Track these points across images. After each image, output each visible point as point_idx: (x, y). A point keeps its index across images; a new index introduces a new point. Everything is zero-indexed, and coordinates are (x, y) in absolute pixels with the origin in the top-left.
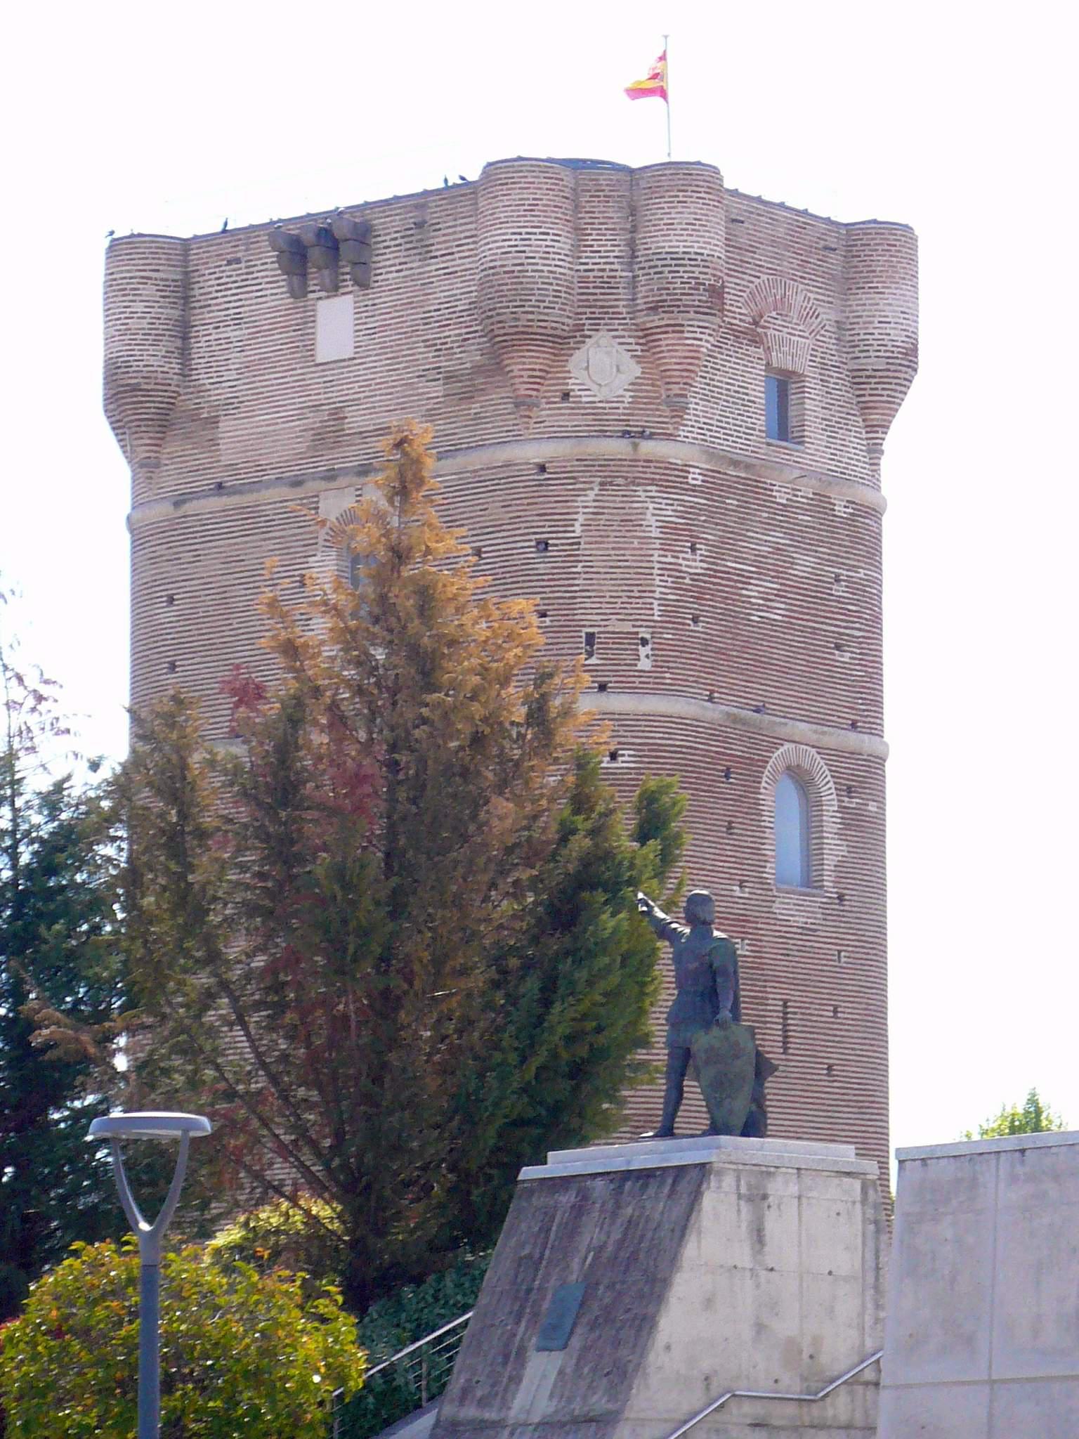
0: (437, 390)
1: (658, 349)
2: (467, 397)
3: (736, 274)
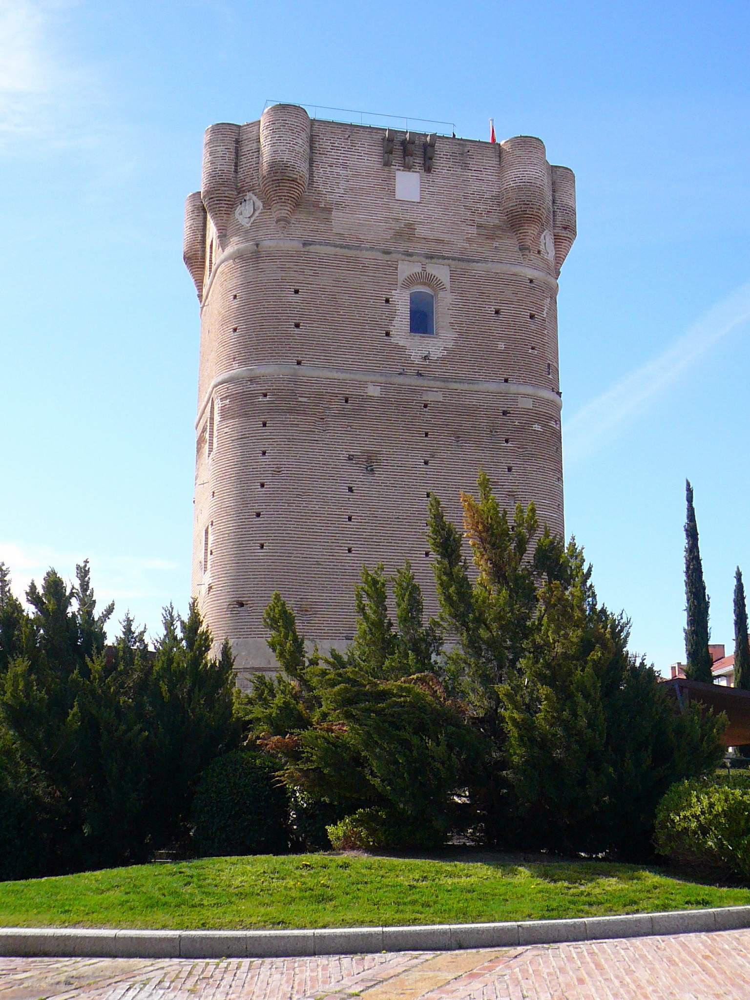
0: (474, 230)
1: (560, 246)
2: (491, 237)
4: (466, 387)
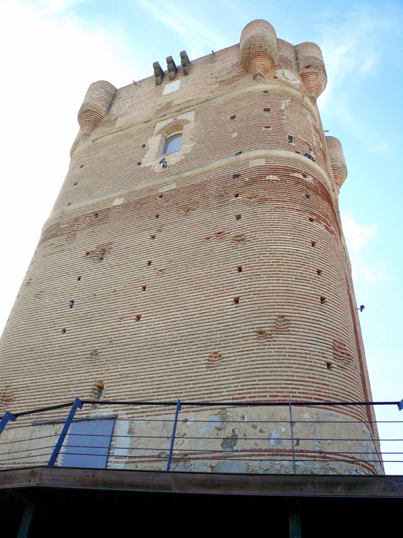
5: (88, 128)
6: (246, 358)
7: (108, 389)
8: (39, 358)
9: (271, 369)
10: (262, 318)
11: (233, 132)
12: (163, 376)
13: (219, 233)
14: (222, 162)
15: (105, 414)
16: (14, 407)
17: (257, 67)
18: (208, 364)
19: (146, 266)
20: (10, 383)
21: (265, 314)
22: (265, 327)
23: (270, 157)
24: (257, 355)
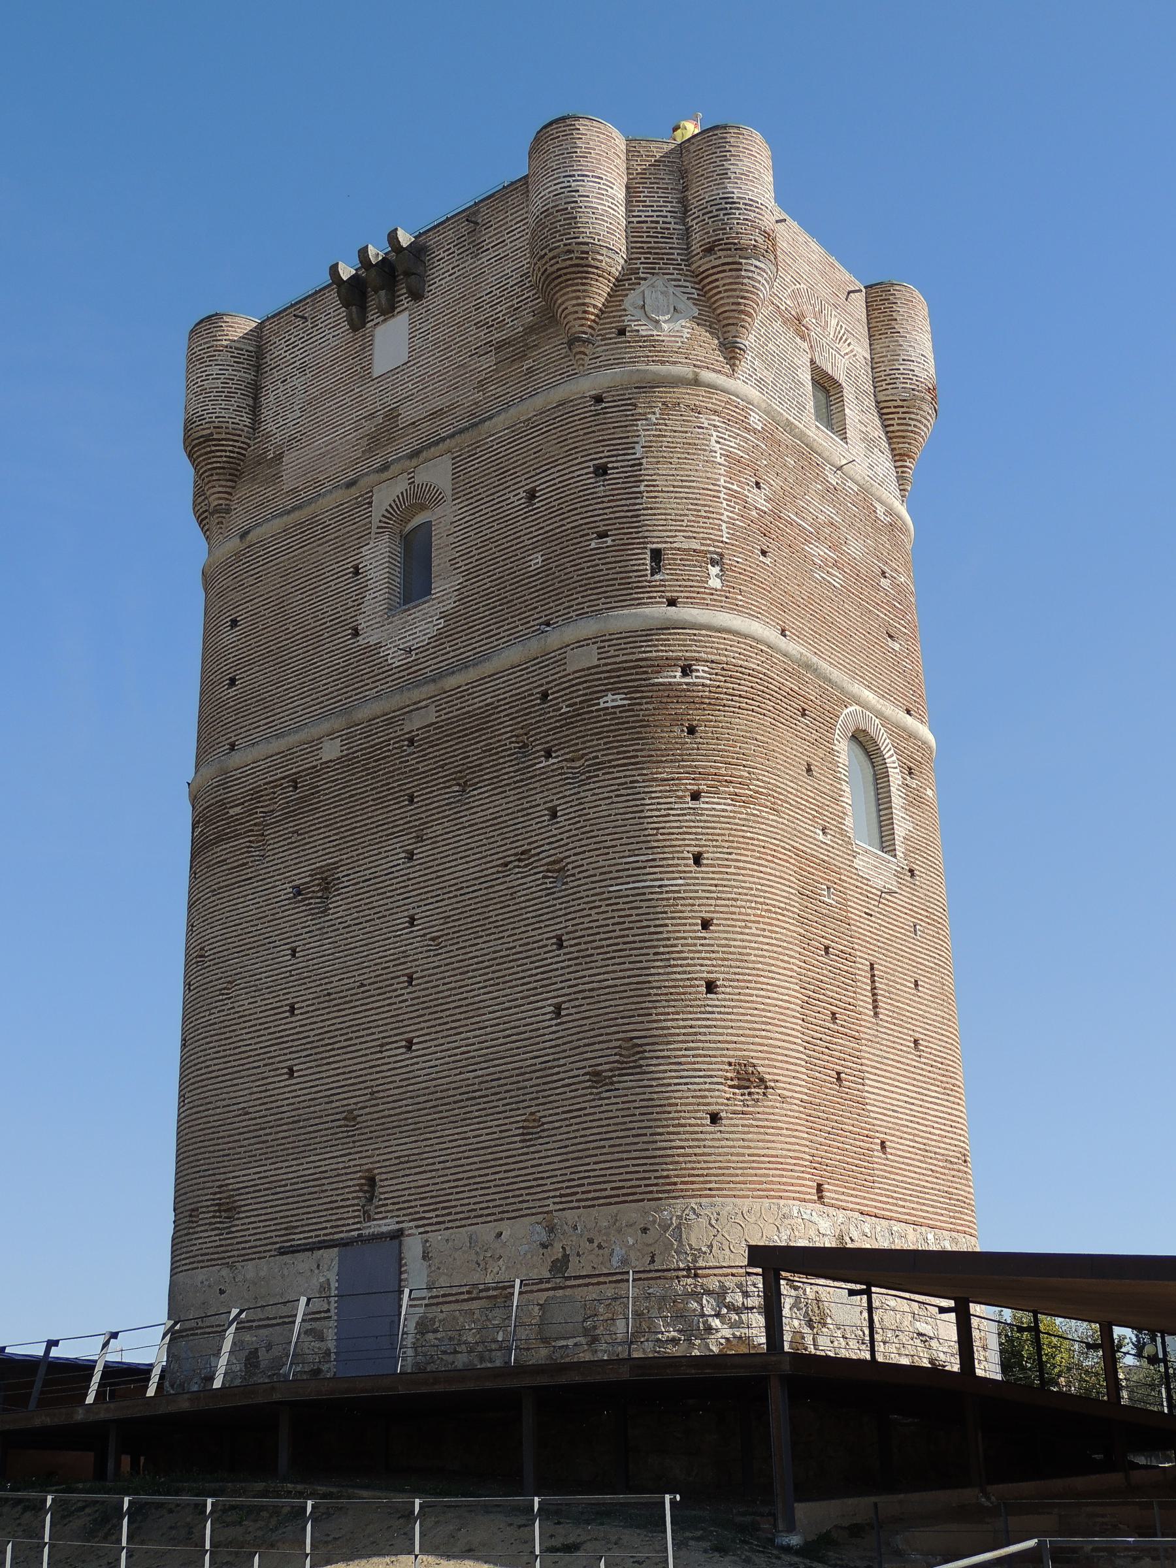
3: (628, 1071)
4: (472, 674)
5: (220, 489)
6: (576, 1124)
7: (382, 1184)
8: (261, 1129)
9: (612, 1142)
10: (597, 1047)
11: (535, 548)
12: (460, 1159)
13: (522, 853)
14: (514, 655)
15: (384, 1229)
16: (242, 1225)
17: (569, 314)
18: (523, 1134)
19: (407, 928)
20: (224, 1180)
21: (601, 1038)
22: (601, 1064)
23: (607, 637)
24: (591, 1118)
